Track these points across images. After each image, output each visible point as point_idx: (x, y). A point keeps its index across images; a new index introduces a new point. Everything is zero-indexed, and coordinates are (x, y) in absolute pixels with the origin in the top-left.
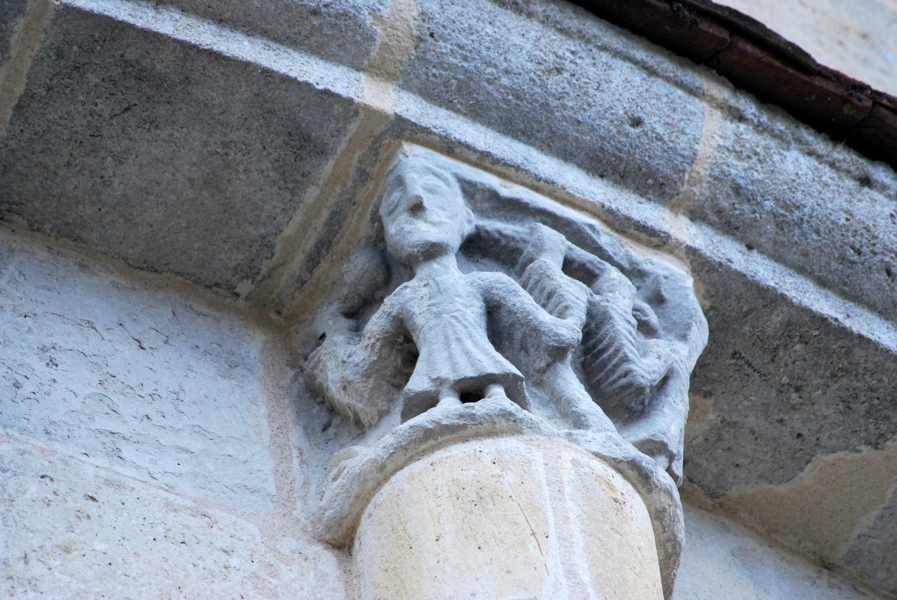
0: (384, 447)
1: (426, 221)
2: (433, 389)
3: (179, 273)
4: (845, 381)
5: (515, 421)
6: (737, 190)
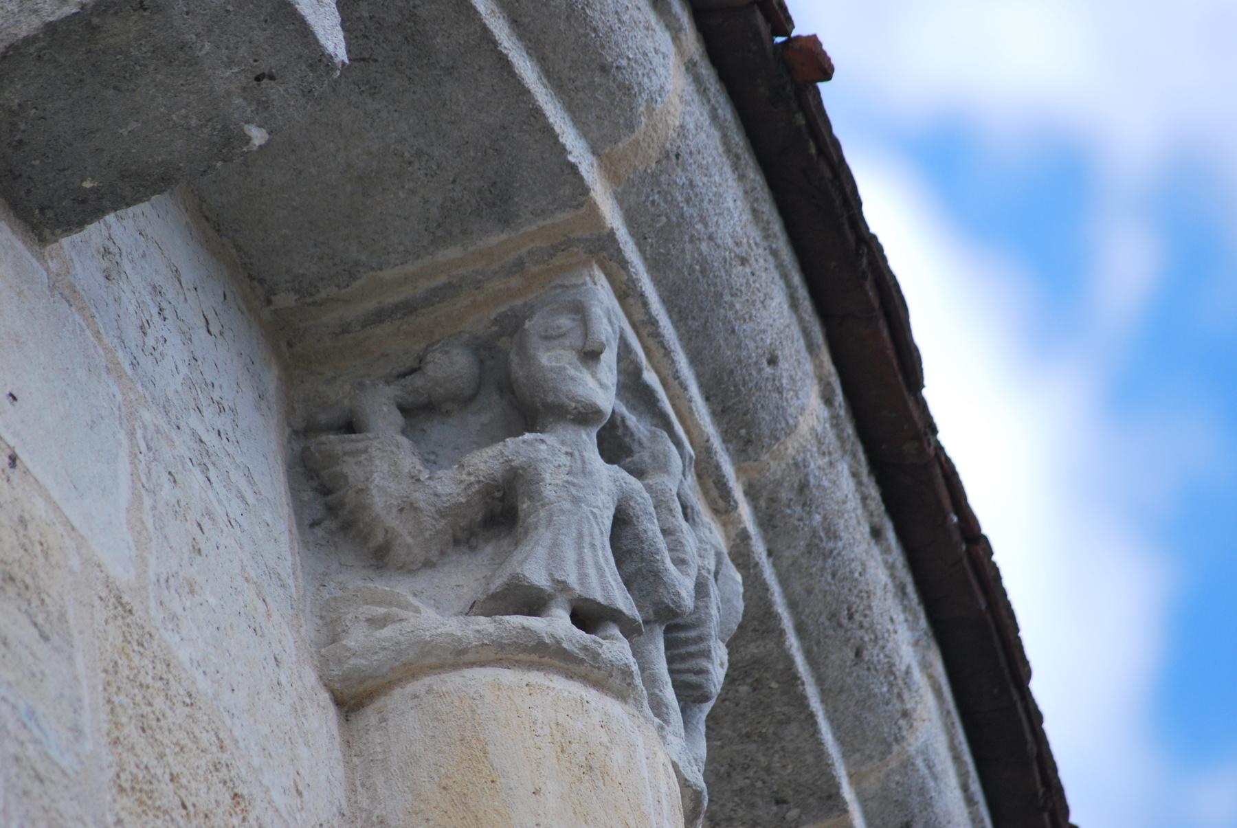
0: (478, 631)
1: (594, 376)
2: (550, 590)
3: (238, 248)
4: (753, 747)
5: (629, 684)
6: (803, 487)
